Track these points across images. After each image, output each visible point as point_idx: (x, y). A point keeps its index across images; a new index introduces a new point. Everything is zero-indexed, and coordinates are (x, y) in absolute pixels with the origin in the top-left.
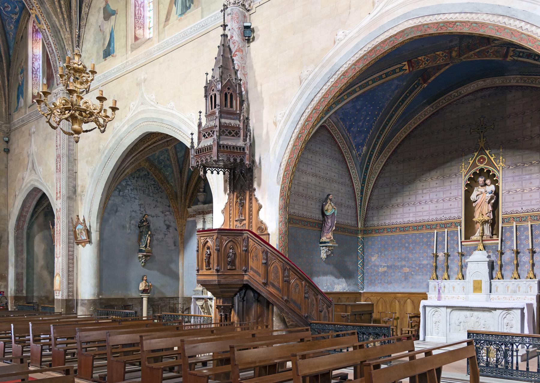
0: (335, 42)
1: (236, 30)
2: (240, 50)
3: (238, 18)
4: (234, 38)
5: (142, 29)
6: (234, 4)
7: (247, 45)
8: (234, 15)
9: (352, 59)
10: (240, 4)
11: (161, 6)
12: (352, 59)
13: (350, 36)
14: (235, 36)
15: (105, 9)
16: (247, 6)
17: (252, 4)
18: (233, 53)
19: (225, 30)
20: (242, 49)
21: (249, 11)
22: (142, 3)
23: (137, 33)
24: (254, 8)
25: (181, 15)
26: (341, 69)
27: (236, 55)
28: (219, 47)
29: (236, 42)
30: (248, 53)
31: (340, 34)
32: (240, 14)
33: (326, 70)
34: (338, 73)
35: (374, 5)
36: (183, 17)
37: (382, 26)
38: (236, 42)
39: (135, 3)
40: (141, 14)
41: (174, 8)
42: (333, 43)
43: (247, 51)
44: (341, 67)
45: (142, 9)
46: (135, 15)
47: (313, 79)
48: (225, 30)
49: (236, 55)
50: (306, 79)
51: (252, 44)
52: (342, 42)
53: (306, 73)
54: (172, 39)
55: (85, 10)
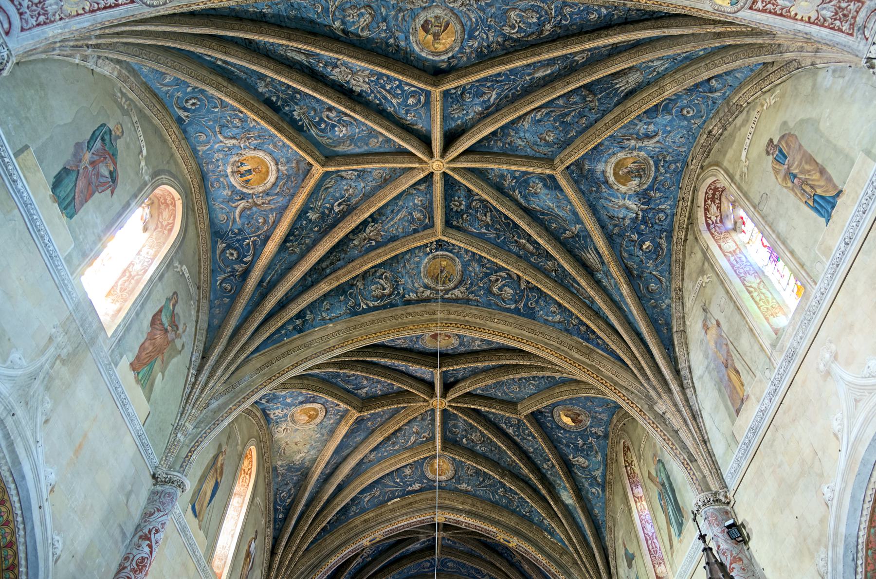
0: (827, 505)
1: (720, 535)
2: (735, 560)
3: (716, 520)
4: (722, 547)
5: (662, 565)
6: (704, 505)
7: (745, 548)
8: (710, 519)
9: (863, 519)
10: (711, 501)
11: (662, 531)
12: (863, 519)
13: (837, 489)
14: (721, 544)
15: (626, 554)
16: (723, 499)
17: (728, 494)
18: (728, 567)
19: (705, 542)
20: (740, 556)
21: (728, 503)
22: (653, 533)
23: (658, 572)
24: (732, 498)
25: (679, 535)
26: (860, 541)
27: (733, 568)
28: (705, 567)
29: (727, 552)
30: (751, 559)
31: (828, 495)
32: (717, 514)
33: (841, 550)
34: (860, 547)
35: (837, 438)
36: (682, 535)
37: (863, 459)
38: (727, 552)
39: (645, 537)
40: (656, 547)
41: (672, 530)
42: (826, 507)
43: (749, 557)
44: (858, 538)
45: (655, 540)
46: (650, 551)
47: (834, 569)
48: (705, 542)
49: (733, 568)
50: (827, 573)
51: (750, 544)
52: (835, 502)
53: (822, 563)
54: (682, 568)
55: (612, 563)
